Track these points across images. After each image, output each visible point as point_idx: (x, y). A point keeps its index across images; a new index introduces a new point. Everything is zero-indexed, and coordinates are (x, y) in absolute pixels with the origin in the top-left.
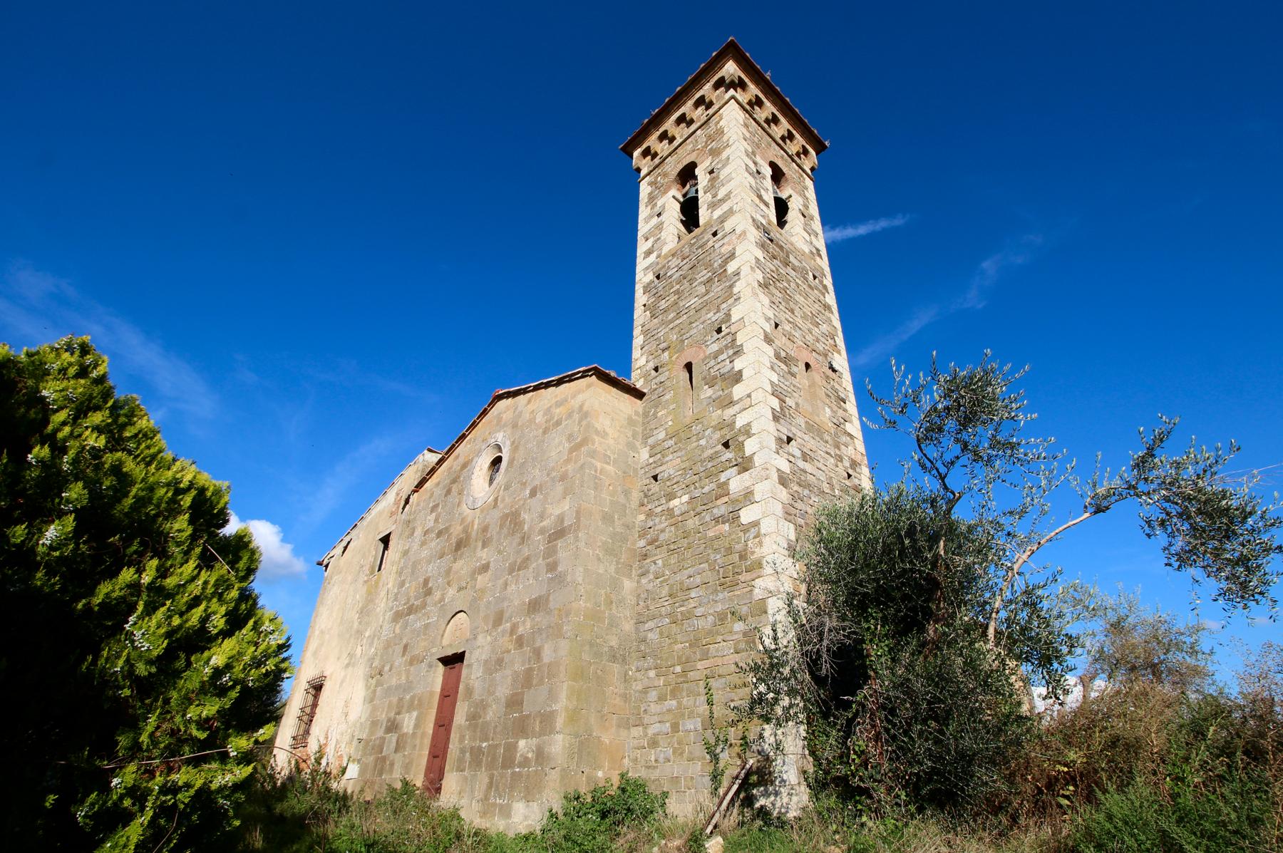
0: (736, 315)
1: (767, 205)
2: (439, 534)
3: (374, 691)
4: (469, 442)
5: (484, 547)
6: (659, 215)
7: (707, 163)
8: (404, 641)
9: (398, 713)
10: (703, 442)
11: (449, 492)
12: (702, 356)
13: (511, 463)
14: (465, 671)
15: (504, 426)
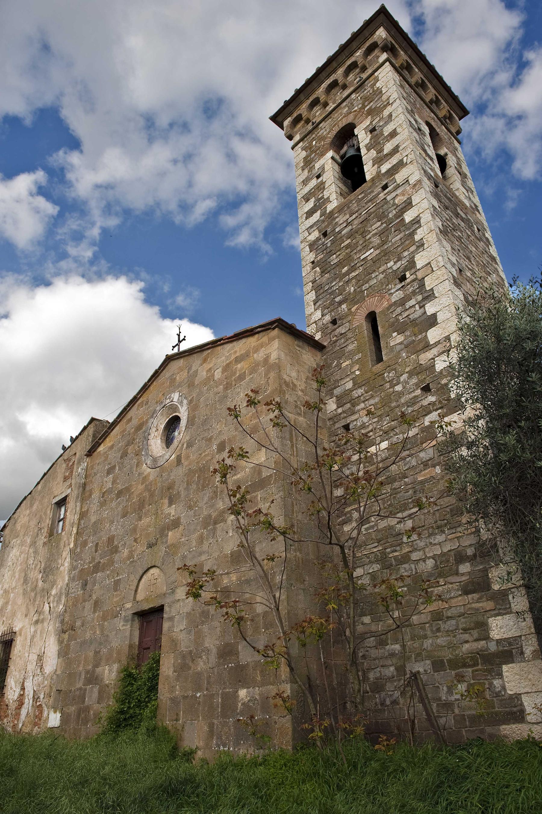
0: (420, 261)
1: (431, 159)
2: (120, 494)
3: (68, 646)
4: (141, 405)
5: (171, 503)
6: (318, 177)
7: (367, 122)
8: (94, 597)
9: (97, 666)
10: (398, 388)
11: (125, 454)
12: (386, 304)
13: (191, 421)
14: (166, 625)
15: (179, 386)
